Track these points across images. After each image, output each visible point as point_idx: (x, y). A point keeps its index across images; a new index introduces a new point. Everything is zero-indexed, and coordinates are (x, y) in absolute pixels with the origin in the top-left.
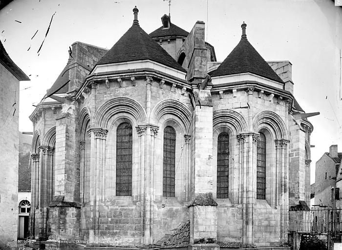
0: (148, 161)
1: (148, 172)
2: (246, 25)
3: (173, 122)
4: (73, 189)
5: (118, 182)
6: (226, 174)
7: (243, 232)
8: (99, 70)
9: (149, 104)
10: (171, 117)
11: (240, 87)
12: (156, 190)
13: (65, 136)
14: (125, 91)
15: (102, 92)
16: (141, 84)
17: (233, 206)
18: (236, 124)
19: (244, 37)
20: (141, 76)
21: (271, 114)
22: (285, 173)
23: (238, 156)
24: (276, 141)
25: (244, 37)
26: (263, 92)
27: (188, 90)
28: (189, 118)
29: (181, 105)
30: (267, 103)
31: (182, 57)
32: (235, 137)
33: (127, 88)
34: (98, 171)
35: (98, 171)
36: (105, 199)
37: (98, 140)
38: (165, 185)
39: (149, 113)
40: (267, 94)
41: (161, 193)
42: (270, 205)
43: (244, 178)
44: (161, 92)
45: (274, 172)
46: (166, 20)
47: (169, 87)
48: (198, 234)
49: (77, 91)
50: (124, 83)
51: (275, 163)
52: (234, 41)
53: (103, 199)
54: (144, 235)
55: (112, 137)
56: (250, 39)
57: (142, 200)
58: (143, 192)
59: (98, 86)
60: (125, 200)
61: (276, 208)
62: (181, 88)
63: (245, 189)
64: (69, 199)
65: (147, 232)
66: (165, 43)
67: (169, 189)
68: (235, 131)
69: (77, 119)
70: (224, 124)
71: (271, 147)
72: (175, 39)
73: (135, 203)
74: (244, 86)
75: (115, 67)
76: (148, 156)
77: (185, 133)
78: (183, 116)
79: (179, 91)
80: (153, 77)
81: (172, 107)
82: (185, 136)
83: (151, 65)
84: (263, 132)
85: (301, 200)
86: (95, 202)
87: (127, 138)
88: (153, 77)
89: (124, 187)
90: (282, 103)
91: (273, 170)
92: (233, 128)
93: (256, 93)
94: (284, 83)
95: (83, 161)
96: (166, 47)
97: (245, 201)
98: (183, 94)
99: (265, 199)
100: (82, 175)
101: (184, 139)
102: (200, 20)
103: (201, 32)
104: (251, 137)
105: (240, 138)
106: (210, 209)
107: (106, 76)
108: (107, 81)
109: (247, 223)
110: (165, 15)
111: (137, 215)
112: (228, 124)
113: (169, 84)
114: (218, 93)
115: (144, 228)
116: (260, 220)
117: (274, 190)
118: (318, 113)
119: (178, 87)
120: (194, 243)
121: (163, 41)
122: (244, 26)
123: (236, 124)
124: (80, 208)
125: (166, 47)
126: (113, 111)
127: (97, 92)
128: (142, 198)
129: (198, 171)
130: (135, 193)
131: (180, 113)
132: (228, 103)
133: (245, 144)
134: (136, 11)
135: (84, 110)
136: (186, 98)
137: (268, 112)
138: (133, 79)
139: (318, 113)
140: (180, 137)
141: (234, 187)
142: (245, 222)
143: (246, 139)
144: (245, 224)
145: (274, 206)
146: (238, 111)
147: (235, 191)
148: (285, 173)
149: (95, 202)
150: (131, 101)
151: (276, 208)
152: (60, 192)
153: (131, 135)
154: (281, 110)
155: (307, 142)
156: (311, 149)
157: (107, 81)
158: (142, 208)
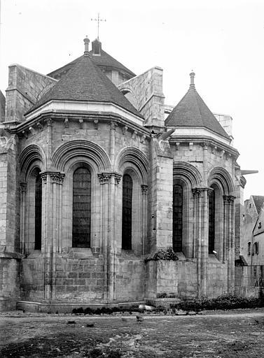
0: (112, 211)
1: (112, 223)
2: (194, 74)
4: (13, 237)
5: (176, 204)
6: (180, 228)
7: (198, 285)
9: (113, 152)
10: (130, 165)
11: (196, 141)
12: (116, 245)
13: (6, 175)
14: (86, 134)
15: (59, 130)
16: (105, 128)
17: (187, 261)
18: (191, 178)
19: (192, 86)
21: (225, 173)
22: (232, 229)
23: (192, 210)
24: (224, 197)
25: (192, 86)
27: (147, 138)
29: (141, 153)
30: (218, 159)
32: (190, 190)
33: (89, 131)
34: (54, 219)
35: (54, 219)
36: (62, 251)
37: (55, 185)
39: (113, 161)
40: (219, 150)
42: (219, 259)
45: (222, 227)
48: (161, 288)
50: (85, 125)
51: (223, 219)
53: (60, 250)
54: (108, 290)
55: (68, 185)
56: (200, 89)
57: (104, 252)
58: (106, 245)
59: (55, 125)
60: (85, 253)
61: (224, 263)
63: (200, 244)
65: (111, 288)
67: (127, 244)
68: (189, 185)
70: (179, 176)
71: (219, 202)
72: (111, 71)
73: (96, 255)
75: (81, 109)
76: (112, 206)
77: (142, 183)
78: (141, 165)
79: (138, 139)
81: (132, 156)
82: (142, 186)
83: (112, 109)
84: (214, 185)
85: (241, 254)
87: (84, 184)
88: (117, 123)
89: (81, 237)
90: (229, 160)
91: (222, 225)
92: (187, 181)
93: (210, 148)
95: (24, 205)
97: (200, 256)
98: (142, 142)
99: (90, 247)
101: (140, 189)
103: (160, 78)
104: (206, 193)
105: (196, 192)
106: (172, 263)
107: (67, 115)
108: (67, 120)
109: (202, 278)
111: (100, 268)
112: (182, 177)
113: (131, 131)
114: (175, 144)
115: (108, 283)
116: (212, 275)
117: (222, 246)
118: (257, 172)
120: (158, 298)
122: (192, 75)
123: (191, 178)
126: (66, 158)
127: (54, 130)
128: (106, 251)
129: (159, 224)
130: (96, 243)
131: (138, 162)
132: (187, 156)
133: (201, 199)
136: (143, 146)
138: (96, 122)
139: (257, 172)
140: (136, 187)
141: (189, 241)
142: (200, 276)
143: (202, 195)
144: (199, 279)
145: (222, 261)
146: (192, 164)
147: (189, 245)
148: (232, 229)
149: (52, 254)
150: (96, 146)
151: (224, 263)
157: (67, 120)
158: (106, 262)
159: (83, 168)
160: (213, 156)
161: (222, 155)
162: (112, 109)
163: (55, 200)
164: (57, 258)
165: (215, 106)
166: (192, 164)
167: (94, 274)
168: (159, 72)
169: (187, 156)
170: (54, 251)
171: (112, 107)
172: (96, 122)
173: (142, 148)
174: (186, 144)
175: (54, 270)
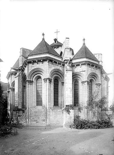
2: (85, 39)
3: (58, 77)
5: (37, 100)
8: (29, 58)
11: (82, 63)
14: (36, 66)
19: (84, 44)
20: (44, 60)
25: (84, 44)
26: (91, 65)
28: (62, 75)
30: (93, 69)
31: (61, 53)
38: (55, 102)
40: (93, 66)
41: (53, 104)
43: (84, 98)
44: (53, 65)
46: (55, 40)
47: (55, 64)
49: (22, 67)
52: (81, 46)
60: (40, 107)
62: (60, 64)
64: (20, 107)
65: (48, 120)
66: (55, 48)
69: (22, 77)
74: (84, 63)
78: (61, 75)
80: (49, 60)
83: (48, 55)
86: (29, 108)
88: (49, 60)
94: (99, 62)
96: (56, 50)
98: (61, 67)
100: (25, 98)
102: (67, 37)
104: (86, 82)
108: (32, 62)
110: (55, 39)
119: (59, 64)
121: (54, 48)
122: (84, 40)
124: (24, 111)
125: (56, 50)
126: (33, 75)
132: (77, 70)
134: (43, 34)
135: (25, 73)
137: (93, 73)
149: (29, 108)
152: (16, 105)
153: (41, 83)
154: (98, 72)
155: (107, 85)
156: (109, 88)
159: (38, 78)
160: (90, 68)
161: (94, 68)
162: (48, 55)
163: (29, 90)
164: (30, 110)
165: (93, 50)
166: (81, 72)
167: (43, 115)
168: (68, 39)
169: (77, 70)
170: (30, 107)
171: (48, 54)
172: (42, 60)
173: (61, 69)
174: (79, 65)
175: (30, 114)
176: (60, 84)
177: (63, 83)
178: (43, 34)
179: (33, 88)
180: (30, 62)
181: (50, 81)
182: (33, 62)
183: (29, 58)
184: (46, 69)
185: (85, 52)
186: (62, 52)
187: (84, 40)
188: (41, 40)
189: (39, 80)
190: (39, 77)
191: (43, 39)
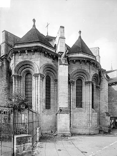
25: (34, 26)
62: (18, 52)
83: (40, 45)
119: (21, 52)
122: (80, 32)
134: (34, 20)
162: (40, 45)
176: (52, 83)
177: (56, 81)
178: (34, 20)
179: (22, 85)
180: (16, 53)
181: (42, 78)
182: (22, 51)
183: (16, 47)
184: (38, 63)
185: (81, 47)
186: (56, 44)
187: (80, 32)
188: (77, 38)
189: (29, 76)
190: (28, 73)
191: (80, 37)
